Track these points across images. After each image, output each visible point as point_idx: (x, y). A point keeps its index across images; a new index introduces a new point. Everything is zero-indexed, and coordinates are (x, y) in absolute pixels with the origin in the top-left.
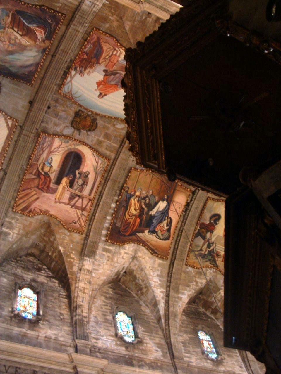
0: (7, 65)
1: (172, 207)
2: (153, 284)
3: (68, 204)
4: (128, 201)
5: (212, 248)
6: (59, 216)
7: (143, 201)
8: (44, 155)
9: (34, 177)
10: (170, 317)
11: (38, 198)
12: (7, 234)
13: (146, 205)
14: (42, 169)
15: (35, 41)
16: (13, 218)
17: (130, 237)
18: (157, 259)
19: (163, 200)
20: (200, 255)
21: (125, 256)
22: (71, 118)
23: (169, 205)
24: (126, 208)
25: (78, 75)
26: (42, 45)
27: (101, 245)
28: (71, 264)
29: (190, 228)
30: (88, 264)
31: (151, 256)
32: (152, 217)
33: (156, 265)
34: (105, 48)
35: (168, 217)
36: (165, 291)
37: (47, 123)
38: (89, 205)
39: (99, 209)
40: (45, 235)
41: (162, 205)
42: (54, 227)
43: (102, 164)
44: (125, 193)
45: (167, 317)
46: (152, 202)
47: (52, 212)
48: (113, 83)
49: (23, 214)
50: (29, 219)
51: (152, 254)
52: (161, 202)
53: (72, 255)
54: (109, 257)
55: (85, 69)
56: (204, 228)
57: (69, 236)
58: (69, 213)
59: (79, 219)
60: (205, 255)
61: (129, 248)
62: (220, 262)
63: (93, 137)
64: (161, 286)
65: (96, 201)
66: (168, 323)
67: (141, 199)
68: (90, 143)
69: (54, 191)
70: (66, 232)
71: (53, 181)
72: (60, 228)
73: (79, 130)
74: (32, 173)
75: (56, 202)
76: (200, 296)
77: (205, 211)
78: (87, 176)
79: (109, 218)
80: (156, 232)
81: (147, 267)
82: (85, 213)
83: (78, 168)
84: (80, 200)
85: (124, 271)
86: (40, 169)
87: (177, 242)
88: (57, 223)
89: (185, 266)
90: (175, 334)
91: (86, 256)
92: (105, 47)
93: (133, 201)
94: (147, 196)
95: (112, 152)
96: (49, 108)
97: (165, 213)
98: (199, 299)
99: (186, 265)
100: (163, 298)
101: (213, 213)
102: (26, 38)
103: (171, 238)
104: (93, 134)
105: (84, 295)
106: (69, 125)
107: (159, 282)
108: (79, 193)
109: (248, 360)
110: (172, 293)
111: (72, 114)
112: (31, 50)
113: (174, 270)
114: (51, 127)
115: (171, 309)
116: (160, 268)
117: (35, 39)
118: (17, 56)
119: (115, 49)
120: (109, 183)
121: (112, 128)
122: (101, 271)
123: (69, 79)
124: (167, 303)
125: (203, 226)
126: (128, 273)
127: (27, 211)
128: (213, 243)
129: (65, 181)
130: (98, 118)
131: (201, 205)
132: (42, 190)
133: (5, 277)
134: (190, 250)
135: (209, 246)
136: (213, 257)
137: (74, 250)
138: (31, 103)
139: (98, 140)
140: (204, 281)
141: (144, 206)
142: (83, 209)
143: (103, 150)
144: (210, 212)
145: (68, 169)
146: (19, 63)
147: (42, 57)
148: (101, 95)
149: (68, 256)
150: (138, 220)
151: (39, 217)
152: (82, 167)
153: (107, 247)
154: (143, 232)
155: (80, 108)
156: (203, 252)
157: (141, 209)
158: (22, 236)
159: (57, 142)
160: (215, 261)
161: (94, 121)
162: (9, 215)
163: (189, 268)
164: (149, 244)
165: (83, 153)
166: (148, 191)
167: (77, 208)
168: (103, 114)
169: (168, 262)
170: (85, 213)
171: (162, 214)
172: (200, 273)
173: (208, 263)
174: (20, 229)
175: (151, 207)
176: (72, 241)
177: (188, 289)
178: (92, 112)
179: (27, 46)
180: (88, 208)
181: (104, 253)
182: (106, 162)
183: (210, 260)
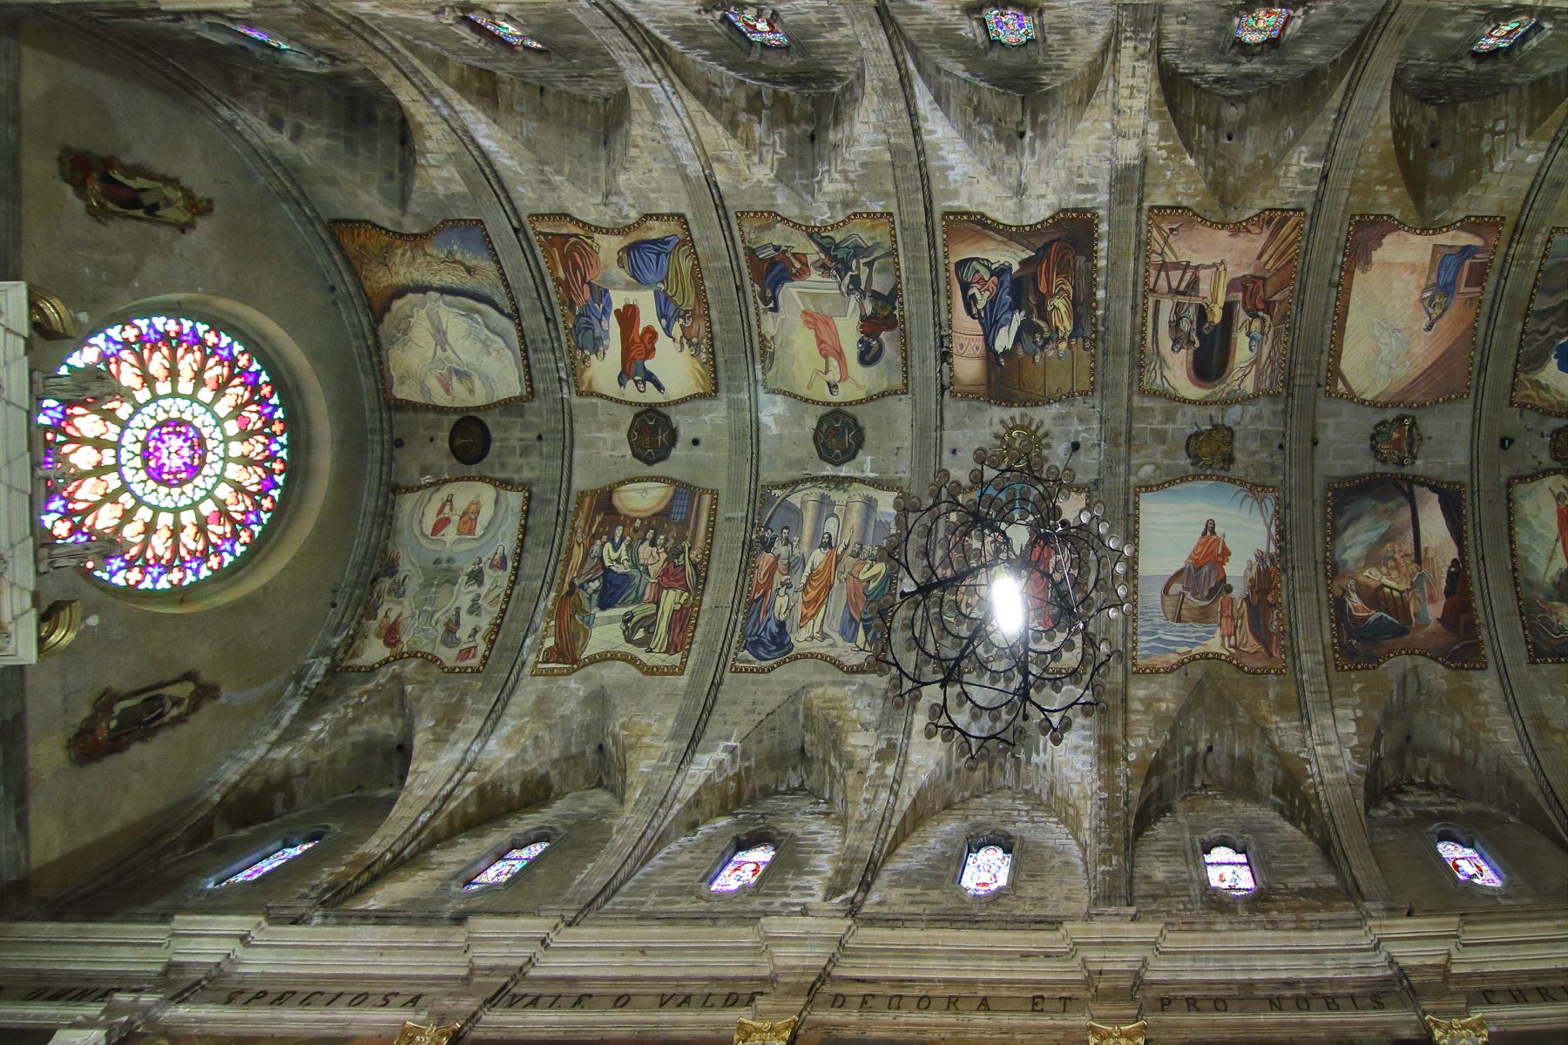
0: (1381, 507)
1: (980, 342)
2: (961, 145)
3: (1197, 268)
4: (1077, 320)
5: (847, 280)
6: (1206, 233)
7: (1047, 335)
8: (1266, 349)
9: (1276, 298)
10: (899, 86)
11: (1259, 257)
12: (1313, 157)
13: (1039, 329)
14: (1263, 321)
15: (1357, 583)
16: (1302, 193)
17: (1046, 240)
18: (968, 207)
19: (1005, 351)
20: (868, 251)
21: (1042, 189)
22: (1237, 444)
23: (989, 346)
24: (1075, 304)
25: (1264, 549)
26: (1343, 582)
27: (1103, 197)
28: (1163, 135)
29: (914, 305)
30: (1129, 150)
31: (981, 209)
32: (1016, 306)
33: (964, 191)
34: (1252, 640)
35: (980, 318)
36: (926, 138)
37: (1275, 413)
38: (1152, 280)
39: (1130, 279)
40: (1224, 170)
41: (1004, 340)
42: (1215, 202)
43: (1153, 379)
44: (1087, 334)
45: (905, 81)
46: (1027, 338)
47: (1224, 234)
48: (1205, 569)
49: (1283, 210)
50: (1269, 205)
51: (983, 215)
52: (1009, 346)
53: (1164, 153)
54: (1080, 176)
55: (1259, 572)
56: (886, 318)
57: (1178, 194)
58: (1189, 248)
59: (1166, 242)
60: (854, 256)
61: (1038, 211)
62: (809, 250)
63: (1185, 423)
64: (936, 147)
65: (1140, 290)
66: (899, 69)
67: (1054, 337)
68: (1188, 409)
69: (1231, 287)
70: (1185, 203)
71: (1239, 306)
72: (1200, 204)
73: (1215, 427)
74: (1281, 302)
75: (1222, 262)
76: (810, 129)
77: (899, 359)
78: (1175, 341)
79: (1102, 263)
80: (993, 273)
81: (982, 180)
82: (1156, 258)
83: (1197, 353)
84: (1174, 284)
85: (1027, 140)
86: (1268, 318)
87: (933, 262)
88: (1208, 215)
89: (893, 209)
90: (878, 50)
91: (1135, 166)
92: (1252, 644)
93: (1067, 325)
94: (1042, 348)
95: (1142, 409)
96: (1281, 447)
97: (990, 327)
98: (809, 119)
99: (890, 214)
100: (926, 120)
101: (882, 362)
102: (1374, 584)
103: (952, 268)
104: (1190, 431)
105: (1131, 82)
106: (1235, 428)
107: (942, 153)
108: (1180, 298)
109: (620, 27)
110: (908, 142)
111: (1238, 455)
112: (1357, 561)
113: (920, 196)
114: (1266, 407)
115: (901, 105)
116: (952, 186)
117: (1362, 590)
118: (1373, 536)
119: (1235, 647)
120: (1127, 344)
121: (1158, 458)
122: (1092, 140)
123: (1273, 530)
124: (913, 115)
125: (890, 323)
126: (1012, 139)
127: (1273, 219)
128: (849, 292)
129: (1217, 316)
130: (1191, 470)
131: (916, 372)
132: (1254, 279)
133: (1313, 57)
134: (893, 253)
135: (855, 281)
136: (834, 259)
137: (1162, 167)
138: (1315, 443)
139: (1174, 422)
140: (828, 187)
141: (1042, 324)
142: (1163, 267)
143: (1158, 405)
144: (888, 362)
145: (1217, 343)
146: (1365, 522)
147: (1332, 552)
148: (1210, 528)
149: (1171, 150)
150: (1043, 288)
151: (1247, 215)
152: (1191, 358)
153: (1089, 196)
154: (1023, 263)
155: (1229, 474)
156: (862, 261)
157: (1044, 316)
158: (1278, 164)
159: (1249, 386)
160: (823, 248)
161: (1195, 458)
162: (1312, 199)
163: (879, 210)
164: (999, 238)
165: (1195, 384)
166: (1044, 359)
167: (1176, 266)
168: (1188, 485)
169: (940, 206)
170: (1156, 258)
171: (997, 322)
172: (846, 204)
173: (838, 238)
174: (1286, 176)
175: (1027, 329)
176: (1169, 184)
177: (865, 158)
178: (1206, 477)
179: (1366, 567)
180: (1153, 273)
181: (1092, 181)
182: (1145, 386)
183: (837, 247)
